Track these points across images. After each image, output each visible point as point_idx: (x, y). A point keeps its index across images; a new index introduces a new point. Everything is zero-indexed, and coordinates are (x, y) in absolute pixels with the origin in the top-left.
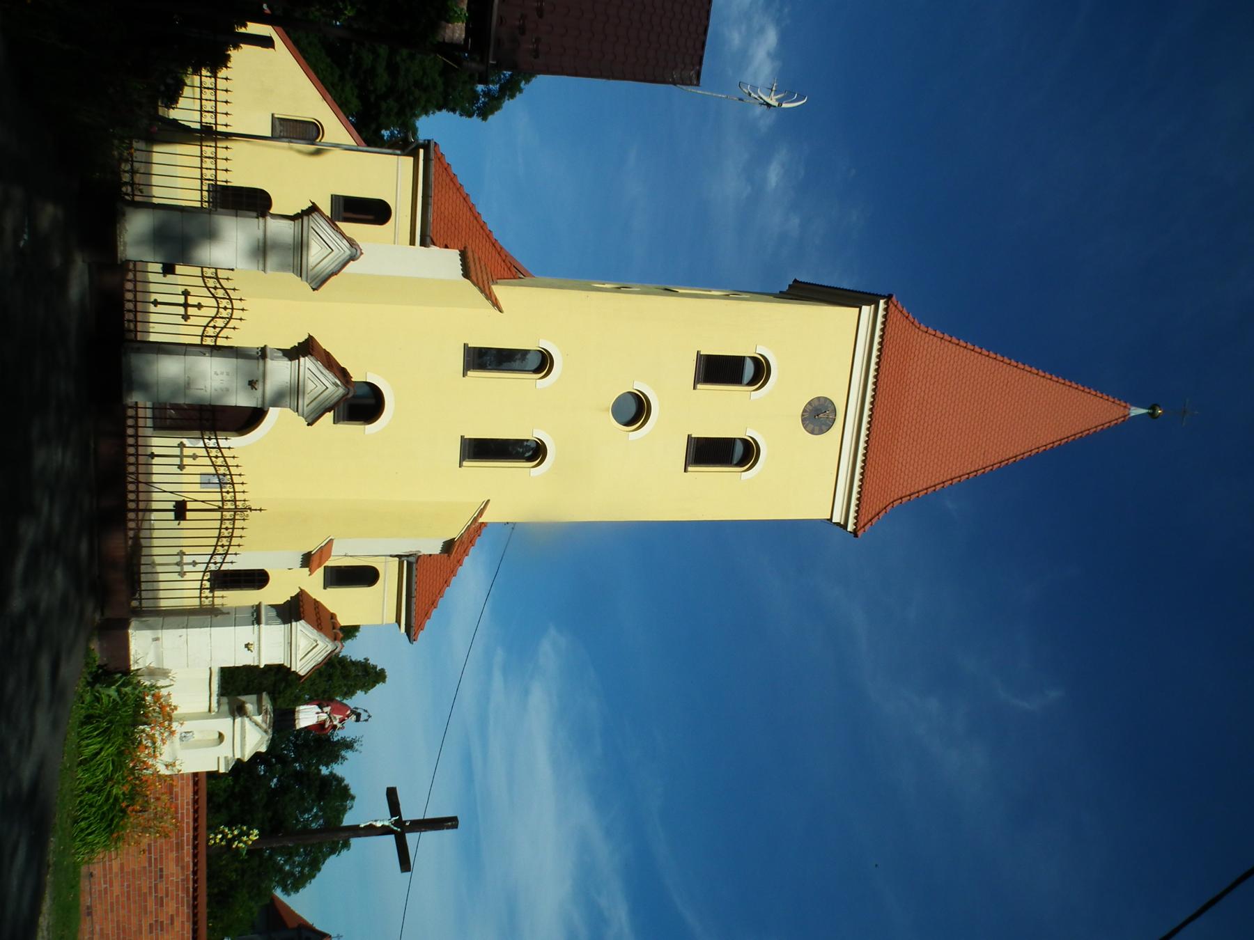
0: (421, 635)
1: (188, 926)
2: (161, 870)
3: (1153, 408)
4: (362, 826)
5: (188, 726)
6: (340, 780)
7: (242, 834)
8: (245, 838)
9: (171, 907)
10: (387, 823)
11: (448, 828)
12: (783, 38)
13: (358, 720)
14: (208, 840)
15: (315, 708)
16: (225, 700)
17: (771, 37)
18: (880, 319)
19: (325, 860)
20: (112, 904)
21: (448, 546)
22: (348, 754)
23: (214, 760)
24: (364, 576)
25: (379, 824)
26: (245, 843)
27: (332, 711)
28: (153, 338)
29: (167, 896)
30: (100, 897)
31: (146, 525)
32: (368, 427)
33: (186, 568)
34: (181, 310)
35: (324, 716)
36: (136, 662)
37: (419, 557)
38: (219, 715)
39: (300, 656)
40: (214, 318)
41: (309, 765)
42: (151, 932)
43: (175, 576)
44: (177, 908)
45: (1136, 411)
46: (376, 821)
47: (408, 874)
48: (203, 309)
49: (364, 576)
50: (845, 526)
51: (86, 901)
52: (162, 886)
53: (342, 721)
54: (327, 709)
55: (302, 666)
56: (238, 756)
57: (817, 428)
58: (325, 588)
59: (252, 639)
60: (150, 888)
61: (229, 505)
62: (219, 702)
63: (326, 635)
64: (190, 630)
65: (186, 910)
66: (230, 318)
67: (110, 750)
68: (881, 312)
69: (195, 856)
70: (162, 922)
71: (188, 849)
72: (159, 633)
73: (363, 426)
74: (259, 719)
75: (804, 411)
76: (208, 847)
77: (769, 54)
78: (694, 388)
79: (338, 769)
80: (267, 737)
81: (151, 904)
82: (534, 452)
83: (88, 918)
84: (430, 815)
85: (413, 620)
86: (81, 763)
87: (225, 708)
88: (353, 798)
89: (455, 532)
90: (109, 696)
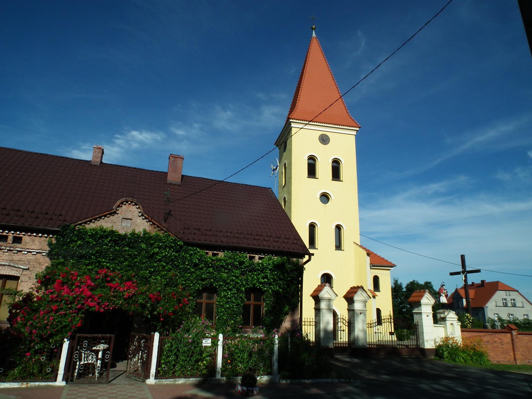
0: (393, 263)
1: (501, 334)
2: (486, 341)
3: (312, 29)
4: (464, 283)
5: (449, 333)
6: (408, 285)
7: (467, 318)
8: (469, 318)
9: (496, 339)
10: (463, 276)
11: (464, 258)
12: (135, 129)
13: (444, 285)
14: (469, 328)
15: (441, 298)
16: (439, 323)
17: (135, 133)
18: (296, 121)
19: (435, 290)
20: (496, 355)
21: (368, 254)
22: (399, 282)
23: (457, 326)
24: (376, 279)
25: (464, 278)
26: (470, 317)
27: (442, 293)
28: (347, 340)
29: (493, 340)
30: (494, 359)
31: (344, 342)
32: (334, 278)
33: (379, 332)
34: (342, 332)
35: (444, 295)
36: (433, 347)
37: (371, 264)
38: (445, 324)
39: (429, 302)
40: (343, 323)
41: (403, 295)
42: (503, 345)
43: (381, 335)
44: (497, 337)
45: (314, 35)
46: (463, 279)
47: (481, 270)
48: (379, 328)
49: (376, 279)
50: (357, 130)
51: (496, 362)
52: (491, 341)
53: (445, 290)
54: (442, 294)
55: (432, 301)
56: (456, 319)
57: (328, 140)
58: (380, 292)
59: (426, 315)
60: (491, 345)
61: (390, 320)
62: (441, 324)
63: (424, 294)
64: (424, 332)
65: (497, 335)
66: (343, 319)
67: (461, 354)
68: (293, 121)
69: (483, 332)
70: (501, 342)
71: (481, 334)
72: (425, 340)
73: (334, 280)
74: (446, 313)
75: (323, 144)
76: (472, 328)
77: (140, 134)
78: (318, 179)
79: (404, 286)
80: (452, 311)
81: (496, 344)
82: (338, 228)
83: (500, 362)
84: (461, 264)
85: (389, 265)
86: (466, 363)
87: (442, 323)
88: (414, 281)
89: (365, 253)
90: (447, 354)
